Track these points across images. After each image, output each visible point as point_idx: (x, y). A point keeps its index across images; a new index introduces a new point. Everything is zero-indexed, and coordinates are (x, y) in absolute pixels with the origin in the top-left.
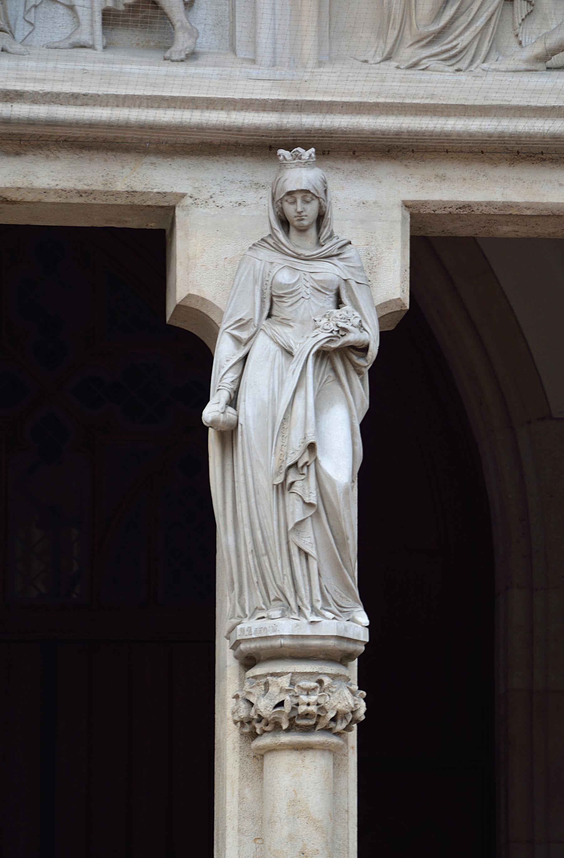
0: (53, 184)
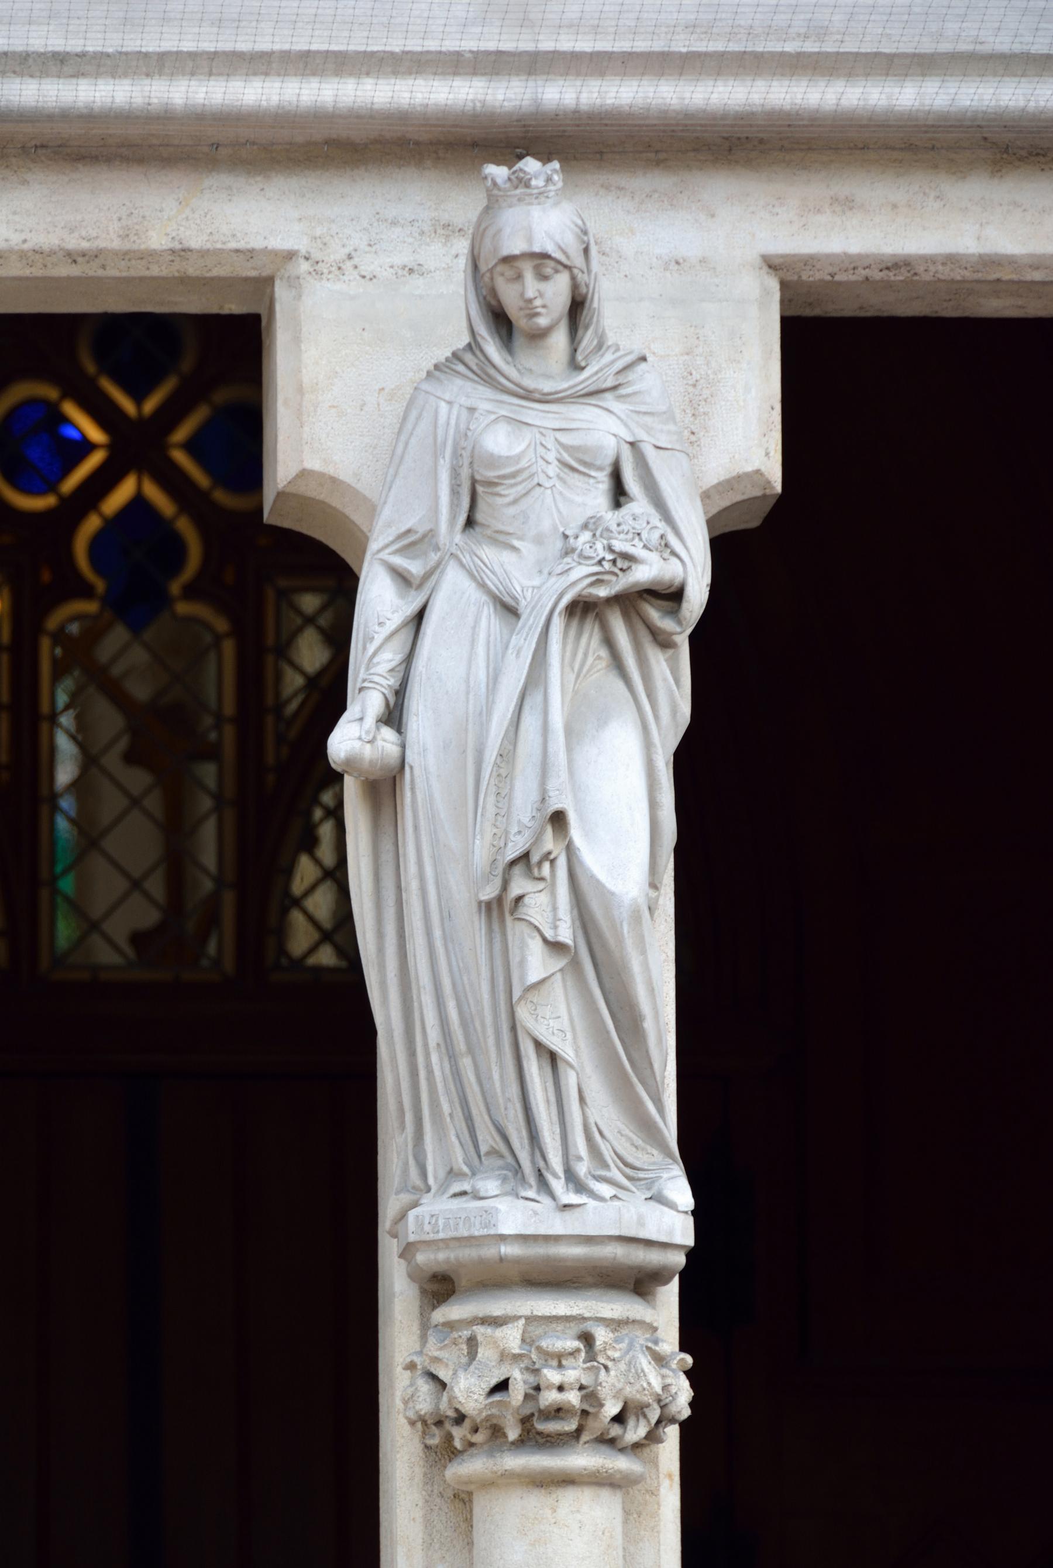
0: (15, 239)
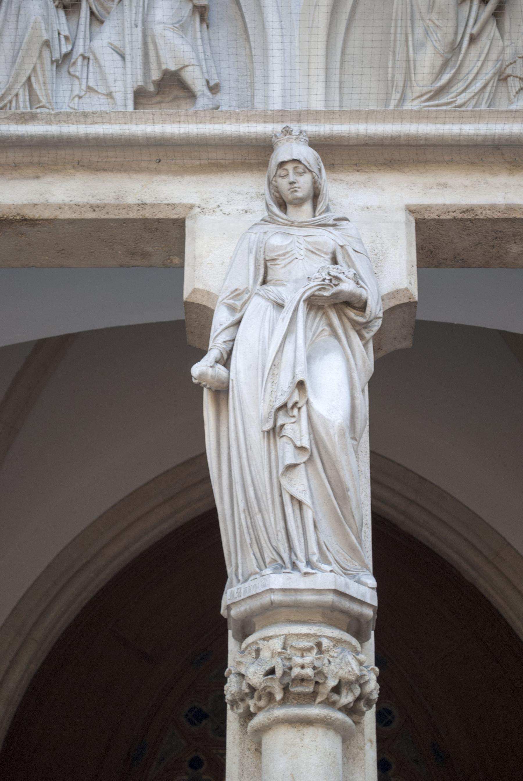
0: (67, 200)
